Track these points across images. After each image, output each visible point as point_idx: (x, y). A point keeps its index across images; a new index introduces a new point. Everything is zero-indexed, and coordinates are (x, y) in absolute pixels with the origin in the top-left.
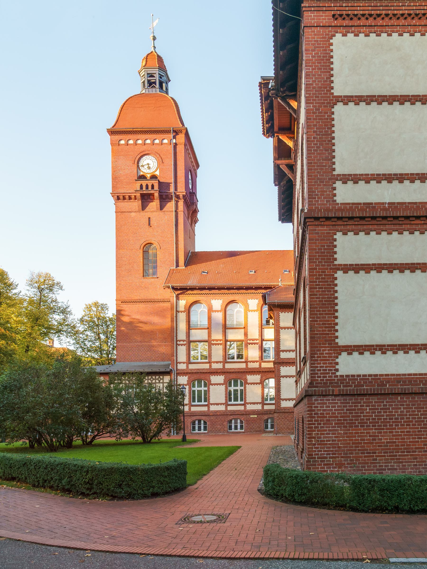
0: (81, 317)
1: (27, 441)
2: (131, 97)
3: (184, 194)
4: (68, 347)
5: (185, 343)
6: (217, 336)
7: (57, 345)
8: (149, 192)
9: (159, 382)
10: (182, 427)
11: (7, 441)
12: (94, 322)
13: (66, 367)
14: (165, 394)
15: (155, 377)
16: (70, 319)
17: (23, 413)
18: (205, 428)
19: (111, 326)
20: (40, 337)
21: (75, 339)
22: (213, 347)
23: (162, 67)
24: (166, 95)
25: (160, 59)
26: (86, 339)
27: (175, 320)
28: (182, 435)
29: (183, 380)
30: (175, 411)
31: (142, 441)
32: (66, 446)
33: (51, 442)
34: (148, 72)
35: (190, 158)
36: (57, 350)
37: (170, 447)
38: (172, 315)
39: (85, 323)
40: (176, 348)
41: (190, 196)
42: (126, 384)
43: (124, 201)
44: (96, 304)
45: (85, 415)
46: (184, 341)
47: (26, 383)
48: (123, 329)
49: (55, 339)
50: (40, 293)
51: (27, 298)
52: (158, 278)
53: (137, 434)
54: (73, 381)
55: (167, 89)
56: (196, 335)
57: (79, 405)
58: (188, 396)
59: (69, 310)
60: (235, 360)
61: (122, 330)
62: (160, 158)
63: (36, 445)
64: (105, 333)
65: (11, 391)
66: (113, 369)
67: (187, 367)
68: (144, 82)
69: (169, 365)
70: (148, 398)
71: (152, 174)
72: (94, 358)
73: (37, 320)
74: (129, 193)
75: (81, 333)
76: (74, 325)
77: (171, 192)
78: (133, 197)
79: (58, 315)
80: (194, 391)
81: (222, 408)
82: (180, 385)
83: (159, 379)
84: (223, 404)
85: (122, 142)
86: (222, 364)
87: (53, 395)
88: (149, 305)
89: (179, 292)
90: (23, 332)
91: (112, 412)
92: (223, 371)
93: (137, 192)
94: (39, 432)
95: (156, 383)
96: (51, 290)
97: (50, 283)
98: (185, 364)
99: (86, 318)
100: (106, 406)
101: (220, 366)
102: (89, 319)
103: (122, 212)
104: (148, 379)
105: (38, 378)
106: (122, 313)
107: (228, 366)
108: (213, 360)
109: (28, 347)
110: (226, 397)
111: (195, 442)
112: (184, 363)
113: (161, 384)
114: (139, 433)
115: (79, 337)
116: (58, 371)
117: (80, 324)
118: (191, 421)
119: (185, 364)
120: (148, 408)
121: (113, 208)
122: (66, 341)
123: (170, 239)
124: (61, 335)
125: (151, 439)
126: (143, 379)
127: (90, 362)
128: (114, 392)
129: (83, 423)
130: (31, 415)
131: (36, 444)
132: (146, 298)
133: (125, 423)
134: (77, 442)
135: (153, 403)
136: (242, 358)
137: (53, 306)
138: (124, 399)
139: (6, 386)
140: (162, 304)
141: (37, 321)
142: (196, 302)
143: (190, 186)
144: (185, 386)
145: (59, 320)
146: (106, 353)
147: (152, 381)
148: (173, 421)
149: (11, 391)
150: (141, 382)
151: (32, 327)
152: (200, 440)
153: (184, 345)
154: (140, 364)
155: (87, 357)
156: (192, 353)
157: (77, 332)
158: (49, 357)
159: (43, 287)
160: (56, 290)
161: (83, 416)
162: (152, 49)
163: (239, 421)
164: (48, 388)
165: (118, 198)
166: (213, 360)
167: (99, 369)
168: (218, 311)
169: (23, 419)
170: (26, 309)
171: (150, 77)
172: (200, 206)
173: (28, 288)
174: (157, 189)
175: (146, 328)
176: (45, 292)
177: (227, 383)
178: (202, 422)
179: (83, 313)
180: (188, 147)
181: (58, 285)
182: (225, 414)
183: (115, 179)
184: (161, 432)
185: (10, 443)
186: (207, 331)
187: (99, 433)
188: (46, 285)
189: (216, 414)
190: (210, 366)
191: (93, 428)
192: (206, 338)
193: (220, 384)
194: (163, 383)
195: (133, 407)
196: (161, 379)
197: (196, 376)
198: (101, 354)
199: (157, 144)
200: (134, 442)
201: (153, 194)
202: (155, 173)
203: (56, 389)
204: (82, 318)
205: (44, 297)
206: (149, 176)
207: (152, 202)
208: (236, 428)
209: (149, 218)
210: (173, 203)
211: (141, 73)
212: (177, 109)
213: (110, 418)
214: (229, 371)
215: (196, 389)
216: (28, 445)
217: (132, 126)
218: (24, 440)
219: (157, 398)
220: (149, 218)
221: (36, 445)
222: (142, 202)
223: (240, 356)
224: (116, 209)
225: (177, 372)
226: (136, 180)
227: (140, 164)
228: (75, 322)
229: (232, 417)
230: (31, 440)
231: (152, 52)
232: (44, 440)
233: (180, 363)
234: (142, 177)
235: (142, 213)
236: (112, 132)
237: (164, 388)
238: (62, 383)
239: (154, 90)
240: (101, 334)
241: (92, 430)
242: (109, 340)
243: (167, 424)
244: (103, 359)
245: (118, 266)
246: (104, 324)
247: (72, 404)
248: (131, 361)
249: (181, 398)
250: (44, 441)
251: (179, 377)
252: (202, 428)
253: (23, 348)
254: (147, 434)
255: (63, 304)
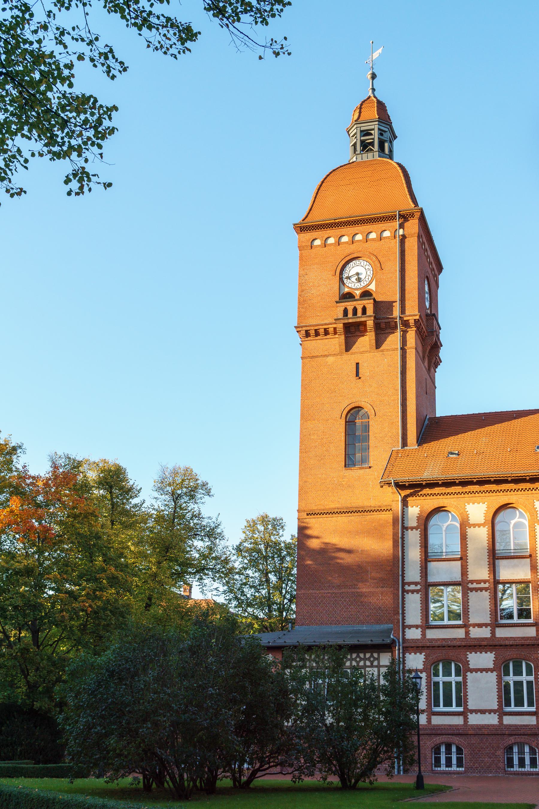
0: (238, 544)
1: (141, 777)
2: (334, 170)
3: (417, 317)
4: (215, 598)
5: (419, 587)
6: (479, 572)
7: (196, 594)
8: (358, 320)
9: (372, 664)
10: (416, 757)
11: (108, 774)
12: (259, 551)
13: (210, 636)
14: (384, 690)
15: (365, 656)
16: (221, 547)
17: (137, 722)
18: (460, 763)
19: (288, 559)
20: (171, 580)
21: (228, 582)
22: (472, 596)
23: (384, 117)
24: (390, 161)
25: (381, 107)
26: (245, 584)
27: (399, 542)
28: (416, 774)
29: (415, 661)
30: (401, 724)
31: (340, 785)
32: (201, 789)
33: (180, 780)
34: (362, 129)
35: (428, 257)
36: (197, 604)
37: (394, 800)
38: (395, 535)
39: (244, 554)
40: (403, 598)
41: (427, 320)
42: (311, 668)
43: (317, 338)
44: (264, 520)
45: (241, 728)
46: (416, 584)
47: (144, 667)
48: (309, 562)
49: (195, 584)
50: (175, 502)
51: (153, 512)
52: (370, 467)
53: (330, 769)
54: (222, 663)
55: (391, 151)
56: (440, 571)
57: (229, 710)
58: (425, 694)
59: (219, 531)
60: (516, 620)
61: (307, 565)
62: (377, 262)
63: (154, 786)
64: (278, 571)
65: (121, 679)
66: (290, 639)
67: (424, 634)
68: (355, 145)
69: (389, 631)
70: (350, 696)
71: (363, 290)
72: (256, 618)
73: (167, 549)
74: (326, 324)
75: (237, 573)
76: (227, 558)
77: (394, 316)
78: (331, 330)
79: (202, 540)
80: (437, 684)
81: (492, 720)
82: (410, 671)
83: (372, 659)
84: (494, 711)
85: (317, 242)
86: (489, 628)
87: (186, 689)
88: (355, 518)
89: (408, 492)
90: (143, 571)
91: (286, 724)
92: (491, 643)
93: (337, 322)
94: (162, 758)
95: (365, 666)
96: (192, 497)
97: (192, 484)
98: (420, 630)
99: (246, 544)
100: (277, 711)
101: (485, 633)
102: (252, 545)
103: (313, 357)
104: (352, 660)
105: (165, 656)
106: (309, 532)
107: (501, 633)
108: (472, 621)
109: (150, 599)
110: (500, 697)
111: (439, 790)
112: (417, 627)
113: (375, 670)
114: (334, 769)
115: (234, 579)
116: (198, 643)
117: (235, 556)
118: (433, 745)
119: (420, 630)
120: (350, 719)
121: (299, 351)
122: (212, 588)
123: (392, 398)
124: (204, 577)
125: (357, 782)
126: (342, 659)
127: (250, 626)
128: (291, 685)
129: (236, 745)
130: (149, 726)
131: (154, 783)
132: (349, 506)
133: (310, 747)
134: (225, 781)
135: (360, 707)
136: (528, 616)
137: (194, 524)
138: (308, 698)
139: (114, 671)
140: (376, 516)
141: (166, 553)
142: (438, 510)
143: (427, 304)
144: (419, 673)
145: (202, 549)
146: (278, 608)
147: (358, 663)
148: (397, 745)
149: (121, 679)
150: (339, 664)
151: (159, 563)
152: (451, 787)
153: (417, 591)
154: (335, 628)
155: (246, 617)
156: (432, 606)
157: (231, 570)
158: (182, 618)
159: (179, 492)
160: (199, 496)
161: (236, 731)
162: (370, 93)
163: (527, 749)
164: (180, 674)
165: (307, 334)
166: (472, 621)
167: (267, 639)
168: (479, 525)
169: (137, 734)
170: (151, 532)
171: (364, 136)
172: (443, 336)
173: (156, 494)
174: (372, 314)
175: (347, 559)
176: (183, 501)
177: (501, 668)
178: (454, 749)
179: (243, 536)
180: (425, 240)
181: (204, 488)
182: (499, 732)
183: (302, 302)
184: (375, 766)
185: (112, 780)
186: (459, 563)
187: (263, 764)
188: (184, 488)
189: (481, 732)
190: (467, 633)
191: (253, 754)
192: (458, 577)
193: (487, 670)
194: (379, 666)
195: (324, 715)
196: (375, 659)
197: (439, 654)
198: (270, 611)
199: (373, 240)
200: (325, 785)
201: (364, 322)
202: (368, 288)
203: (193, 677)
204: (240, 545)
205: (181, 509)
206: (358, 293)
207: (363, 336)
208: (522, 763)
209: (357, 364)
210: (398, 334)
211: (350, 132)
212: (406, 180)
213: (283, 735)
214: (503, 643)
215: (441, 679)
216: (141, 785)
217: (333, 216)
218: (136, 775)
219: (368, 697)
220: (357, 364)
221: (154, 786)
222: (346, 337)
223: (524, 613)
224: (303, 353)
225: (405, 645)
226: (337, 302)
227: (345, 275)
228: (229, 553)
229: (512, 740)
230: (147, 775)
231: (369, 97)
232: (169, 774)
233: (410, 627)
234: (348, 296)
235: (347, 356)
236: (302, 228)
237: (381, 677)
238: (204, 665)
239: (370, 155)
240: (271, 572)
241: (251, 759)
242: (284, 585)
243: (387, 751)
244: (272, 620)
245: (304, 451)
246: (276, 556)
247: (218, 705)
248: (322, 624)
249: (412, 699)
250: (168, 778)
251: (407, 655)
252: (454, 761)
253: (142, 600)
254: (349, 770)
255: (210, 521)
